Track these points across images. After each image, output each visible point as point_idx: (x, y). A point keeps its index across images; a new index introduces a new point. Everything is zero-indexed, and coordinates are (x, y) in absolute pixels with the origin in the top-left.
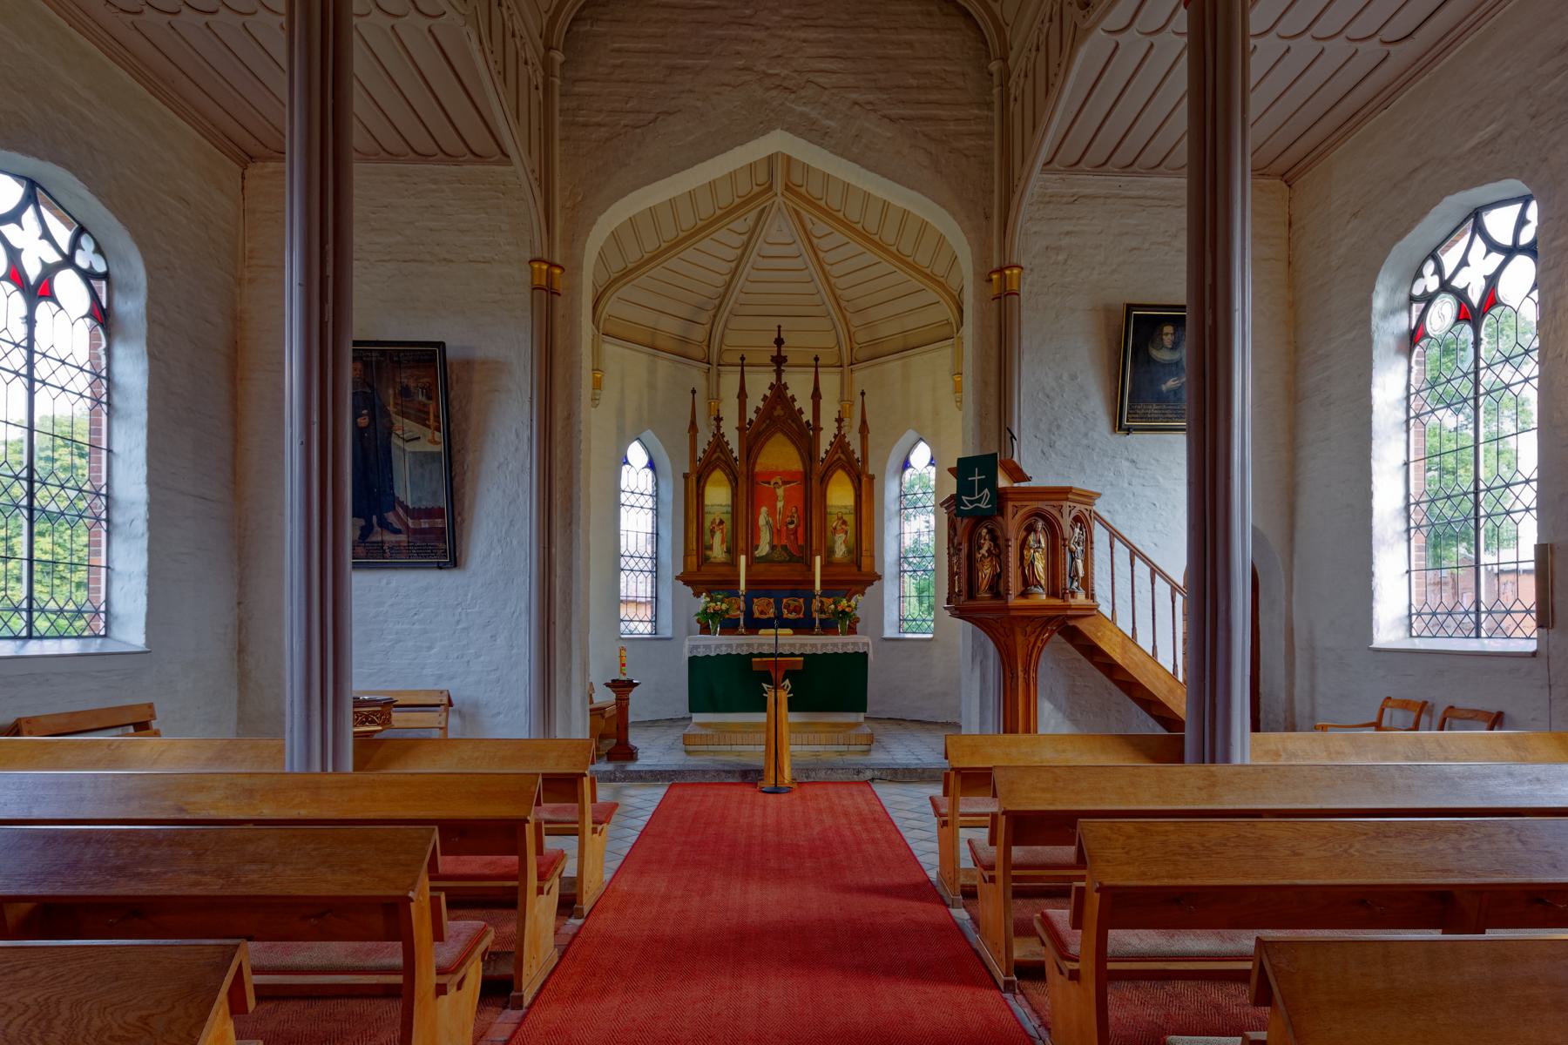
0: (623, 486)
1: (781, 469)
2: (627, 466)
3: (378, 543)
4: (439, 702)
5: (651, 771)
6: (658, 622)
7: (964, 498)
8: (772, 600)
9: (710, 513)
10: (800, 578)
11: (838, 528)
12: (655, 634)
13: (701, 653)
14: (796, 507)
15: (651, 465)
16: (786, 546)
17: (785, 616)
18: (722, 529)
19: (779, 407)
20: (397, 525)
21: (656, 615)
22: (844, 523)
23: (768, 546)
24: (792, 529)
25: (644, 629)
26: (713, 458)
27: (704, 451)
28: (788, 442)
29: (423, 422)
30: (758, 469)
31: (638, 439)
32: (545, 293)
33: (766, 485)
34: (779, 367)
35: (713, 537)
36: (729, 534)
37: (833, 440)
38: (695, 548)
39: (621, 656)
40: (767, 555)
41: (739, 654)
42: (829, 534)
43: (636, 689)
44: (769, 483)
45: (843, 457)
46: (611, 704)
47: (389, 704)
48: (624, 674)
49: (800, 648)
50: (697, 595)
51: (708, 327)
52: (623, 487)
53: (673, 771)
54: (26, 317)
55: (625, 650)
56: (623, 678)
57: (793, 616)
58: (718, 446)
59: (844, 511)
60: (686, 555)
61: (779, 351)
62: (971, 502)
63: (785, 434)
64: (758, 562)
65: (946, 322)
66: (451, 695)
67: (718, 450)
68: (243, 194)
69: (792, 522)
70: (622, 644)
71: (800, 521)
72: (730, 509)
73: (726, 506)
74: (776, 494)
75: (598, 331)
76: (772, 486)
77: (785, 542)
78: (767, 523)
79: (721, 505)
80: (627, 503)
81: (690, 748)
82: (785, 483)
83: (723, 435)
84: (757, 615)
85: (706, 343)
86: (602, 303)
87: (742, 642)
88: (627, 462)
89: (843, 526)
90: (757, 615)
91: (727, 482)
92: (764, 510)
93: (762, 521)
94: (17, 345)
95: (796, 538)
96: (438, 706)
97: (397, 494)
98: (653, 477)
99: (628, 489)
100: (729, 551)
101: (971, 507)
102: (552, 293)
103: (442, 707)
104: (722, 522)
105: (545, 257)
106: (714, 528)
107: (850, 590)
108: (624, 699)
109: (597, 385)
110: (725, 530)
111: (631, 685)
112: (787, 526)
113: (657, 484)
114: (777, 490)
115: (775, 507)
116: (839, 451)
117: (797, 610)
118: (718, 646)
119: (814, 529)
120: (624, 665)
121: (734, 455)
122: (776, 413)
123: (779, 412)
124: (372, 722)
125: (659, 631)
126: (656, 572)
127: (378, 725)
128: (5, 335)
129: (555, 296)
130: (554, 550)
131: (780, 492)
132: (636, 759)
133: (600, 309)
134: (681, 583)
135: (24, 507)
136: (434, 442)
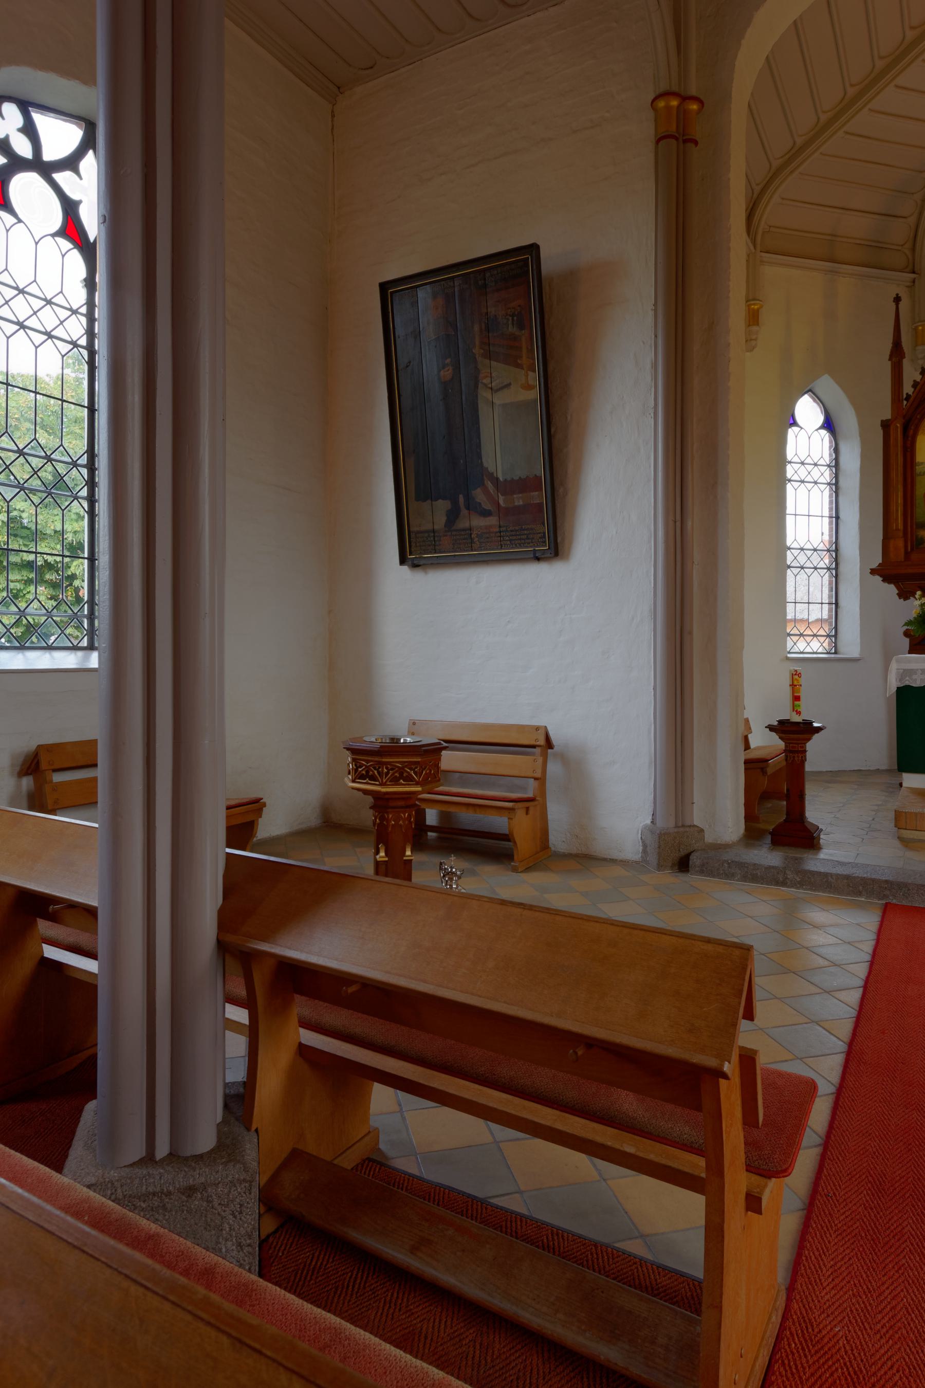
0: (790, 454)
2: (795, 429)
3: (464, 530)
4: (532, 743)
5: (847, 877)
6: (840, 636)
12: (836, 653)
15: (829, 425)
20: (487, 506)
21: (836, 628)
25: (816, 647)
29: (513, 360)
31: (810, 391)
32: (673, 141)
38: (901, 526)
43: (816, 737)
46: (779, 752)
47: (433, 751)
52: (789, 457)
53: (886, 882)
54: (85, 280)
56: (797, 719)
66: (551, 734)
68: (333, 135)
75: (755, 247)
80: (796, 477)
81: (907, 834)
86: (758, 213)
88: (794, 423)
94: (74, 312)
96: (534, 747)
97: (485, 464)
98: (830, 442)
99: (796, 459)
102: (685, 141)
103: (538, 750)
105: (675, 88)
108: (798, 752)
109: (753, 318)
111: (807, 730)
113: (836, 450)
124: (409, 779)
125: (841, 648)
126: (836, 568)
127: (417, 783)
128: (5, 278)
129: (690, 145)
130: (689, 524)
133: (756, 218)
134: (878, 579)
135: (83, 498)
136: (529, 387)
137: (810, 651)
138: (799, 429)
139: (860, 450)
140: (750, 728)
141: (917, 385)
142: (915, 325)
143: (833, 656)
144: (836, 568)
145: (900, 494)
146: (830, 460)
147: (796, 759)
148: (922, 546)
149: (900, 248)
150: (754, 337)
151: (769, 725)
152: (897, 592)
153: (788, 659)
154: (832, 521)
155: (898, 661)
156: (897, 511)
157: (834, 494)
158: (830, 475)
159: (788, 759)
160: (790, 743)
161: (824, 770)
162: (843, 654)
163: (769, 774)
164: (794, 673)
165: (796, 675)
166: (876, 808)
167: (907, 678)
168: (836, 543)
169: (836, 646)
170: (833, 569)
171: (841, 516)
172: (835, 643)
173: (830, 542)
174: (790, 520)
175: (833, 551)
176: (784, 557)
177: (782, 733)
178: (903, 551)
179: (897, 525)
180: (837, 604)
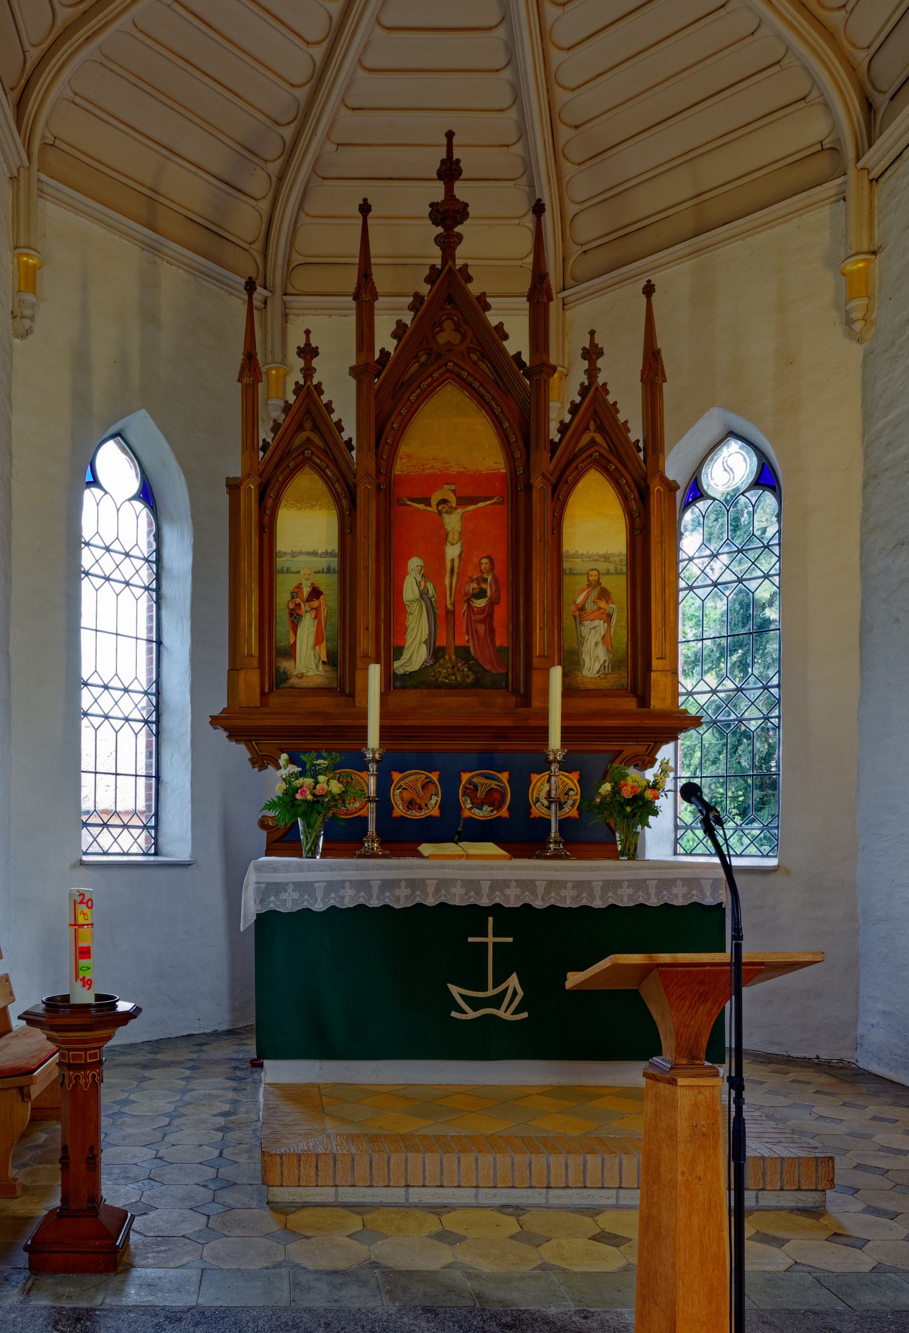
0: (87, 533)
1: (454, 469)
2: (95, 490)
6: (163, 827)
7: (455, 990)
8: (434, 776)
9: (288, 571)
10: (507, 723)
11: (590, 607)
12: (156, 854)
13: (288, 903)
14: (492, 561)
16: (467, 649)
17: (466, 814)
18: (317, 610)
19: (448, 325)
21: (157, 815)
22: (604, 594)
23: (424, 648)
24: (482, 610)
26: (297, 441)
27: (276, 428)
28: (471, 405)
30: (400, 468)
33: (421, 506)
34: (449, 228)
35: (295, 628)
36: (335, 619)
37: (578, 399)
38: (255, 650)
39: (76, 924)
40: (423, 669)
41: (386, 907)
42: (568, 621)
44: (427, 502)
45: (599, 438)
48: (87, 983)
49: (547, 892)
50: (261, 761)
51: (264, 205)
52: (85, 674)
55: (89, 903)
57: (484, 813)
58: (308, 411)
59: (602, 566)
60: (234, 669)
61: (449, 190)
62: (475, 1004)
63: (466, 385)
64: (403, 687)
65: (818, 147)
67: (308, 425)
69: (481, 594)
70: (85, 884)
71: (498, 590)
72: (334, 562)
73: (327, 554)
74: (442, 525)
76: (433, 509)
77: (463, 639)
78: (423, 594)
79: (314, 553)
82: (463, 501)
83: (319, 388)
84: (399, 810)
85: (258, 246)
87: (336, 876)
88: (95, 482)
89: (602, 604)
90: (399, 810)
91: (328, 499)
92: (415, 563)
93: (410, 590)
95: (491, 631)
98: (150, 524)
100: (332, 661)
101: (471, 1014)
104: (316, 593)
106: (298, 606)
107: (621, 752)
108: (85, 1067)
110: (323, 613)
112: (468, 601)
113: (158, 537)
114: (446, 517)
115: (440, 556)
116: (592, 426)
117: (493, 798)
118: (331, 886)
119: (537, 607)
120: (84, 953)
121: (345, 436)
122: (442, 339)
123: (447, 335)
125: (165, 847)
131: (453, 522)
132: (129, 1267)
137: (118, 850)
138: (102, 493)
139: (192, 541)
140: (11, 993)
141: (278, 429)
142: (267, 366)
143: (152, 858)
144: (158, 722)
145: (255, 598)
146: (148, 552)
147: (82, 1081)
148: (285, 685)
149: (246, 246)
150: (28, 312)
151: (26, 1013)
152: (249, 756)
153: (83, 863)
154: (152, 648)
155: (258, 869)
156: (250, 625)
157: (154, 605)
158: (149, 576)
159: (66, 1081)
160: (69, 1050)
161: (140, 1041)
162: (170, 856)
163: (33, 1097)
164: (79, 899)
165: (81, 902)
166: (221, 1121)
167: (272, 898)
168: (158, 682)
169: (156, 844)
170: (152, 722)
171: (164, 642)
172: (156, 838)
173: (149, 681)
174: (86, 638)
175: (152, 694)
176: (78, 698)
177: (51, 1030)
178: (258, 690)
179: (250, 648)
180: (158, 778)
